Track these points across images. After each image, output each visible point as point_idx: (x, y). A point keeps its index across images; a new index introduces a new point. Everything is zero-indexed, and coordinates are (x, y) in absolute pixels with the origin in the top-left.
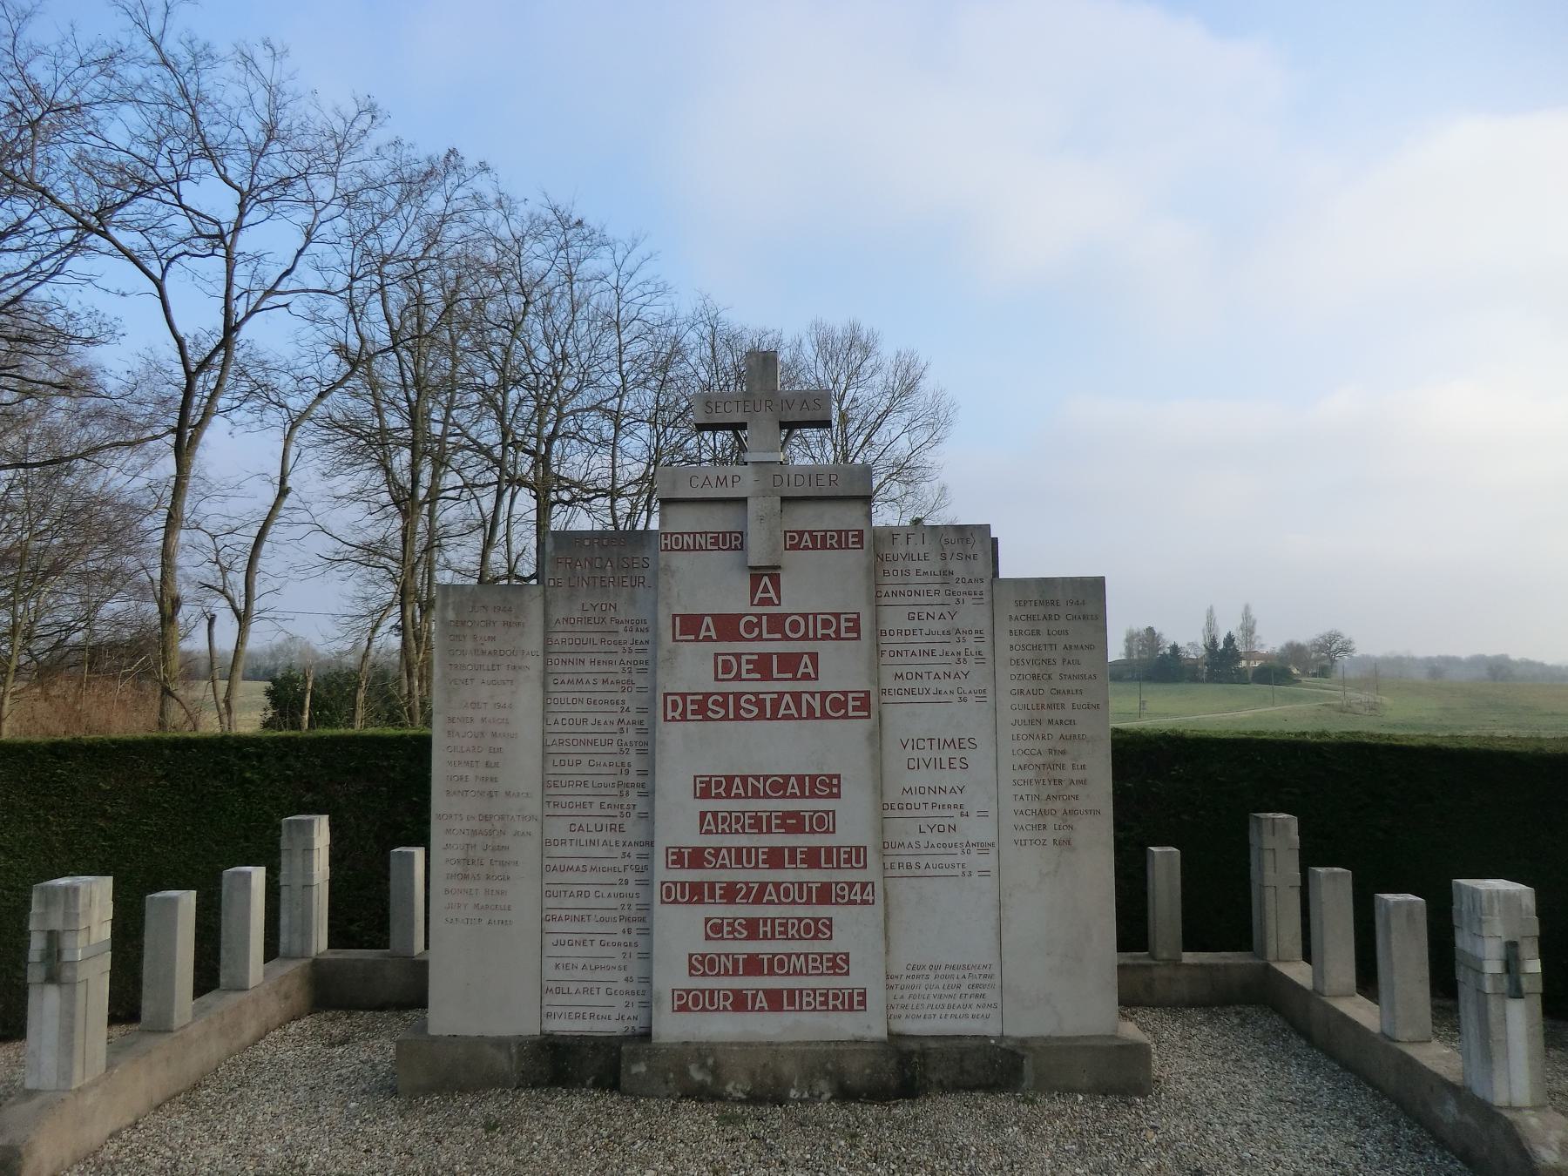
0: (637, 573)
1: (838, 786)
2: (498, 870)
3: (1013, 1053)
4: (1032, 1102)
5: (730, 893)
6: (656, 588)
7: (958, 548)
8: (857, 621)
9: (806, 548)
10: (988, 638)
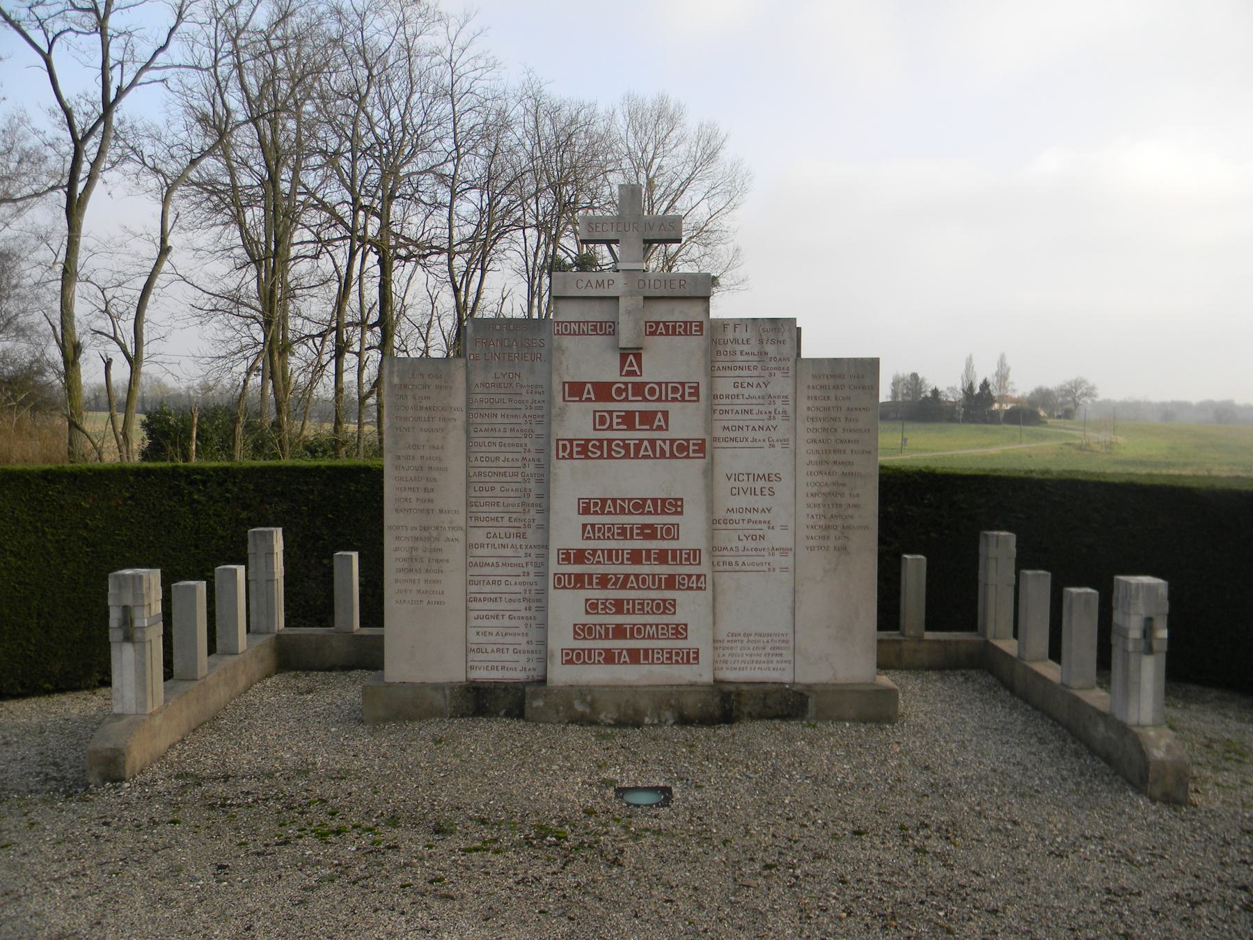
0: (535, 350)
1: (682, 506)
2: (434, 566)
3: (801, 694)
4: (814, 726)
5: (604, 581)
6: (550, 362)
7: (772, 335)
8: (697, 388)
9: (661, 334)
10: (791, 403)
